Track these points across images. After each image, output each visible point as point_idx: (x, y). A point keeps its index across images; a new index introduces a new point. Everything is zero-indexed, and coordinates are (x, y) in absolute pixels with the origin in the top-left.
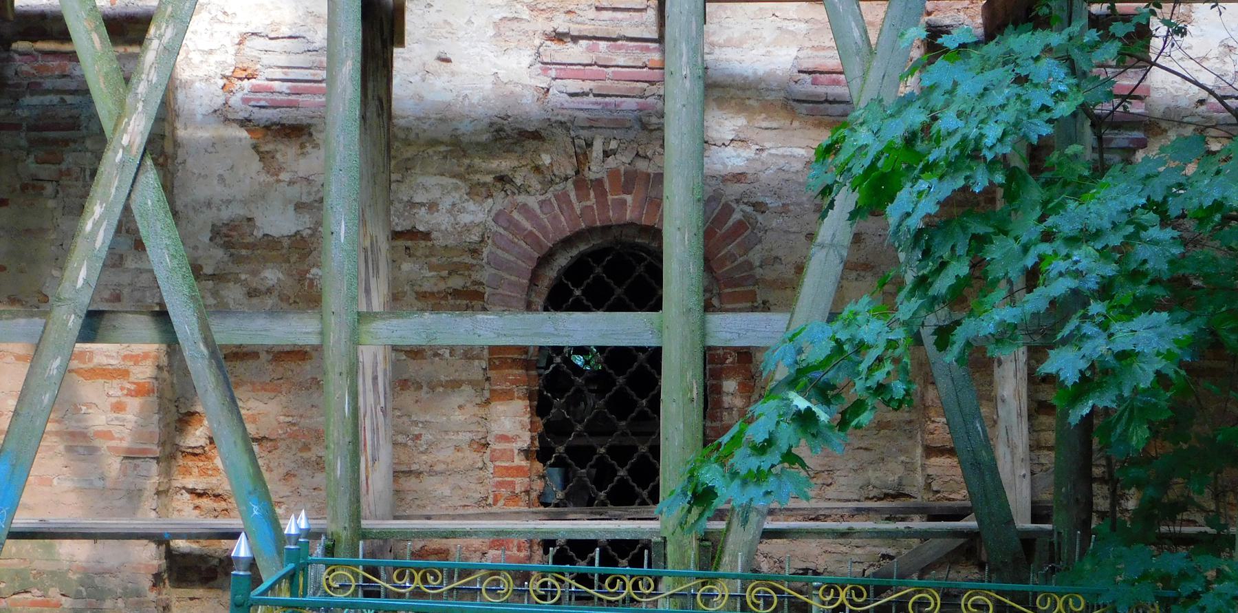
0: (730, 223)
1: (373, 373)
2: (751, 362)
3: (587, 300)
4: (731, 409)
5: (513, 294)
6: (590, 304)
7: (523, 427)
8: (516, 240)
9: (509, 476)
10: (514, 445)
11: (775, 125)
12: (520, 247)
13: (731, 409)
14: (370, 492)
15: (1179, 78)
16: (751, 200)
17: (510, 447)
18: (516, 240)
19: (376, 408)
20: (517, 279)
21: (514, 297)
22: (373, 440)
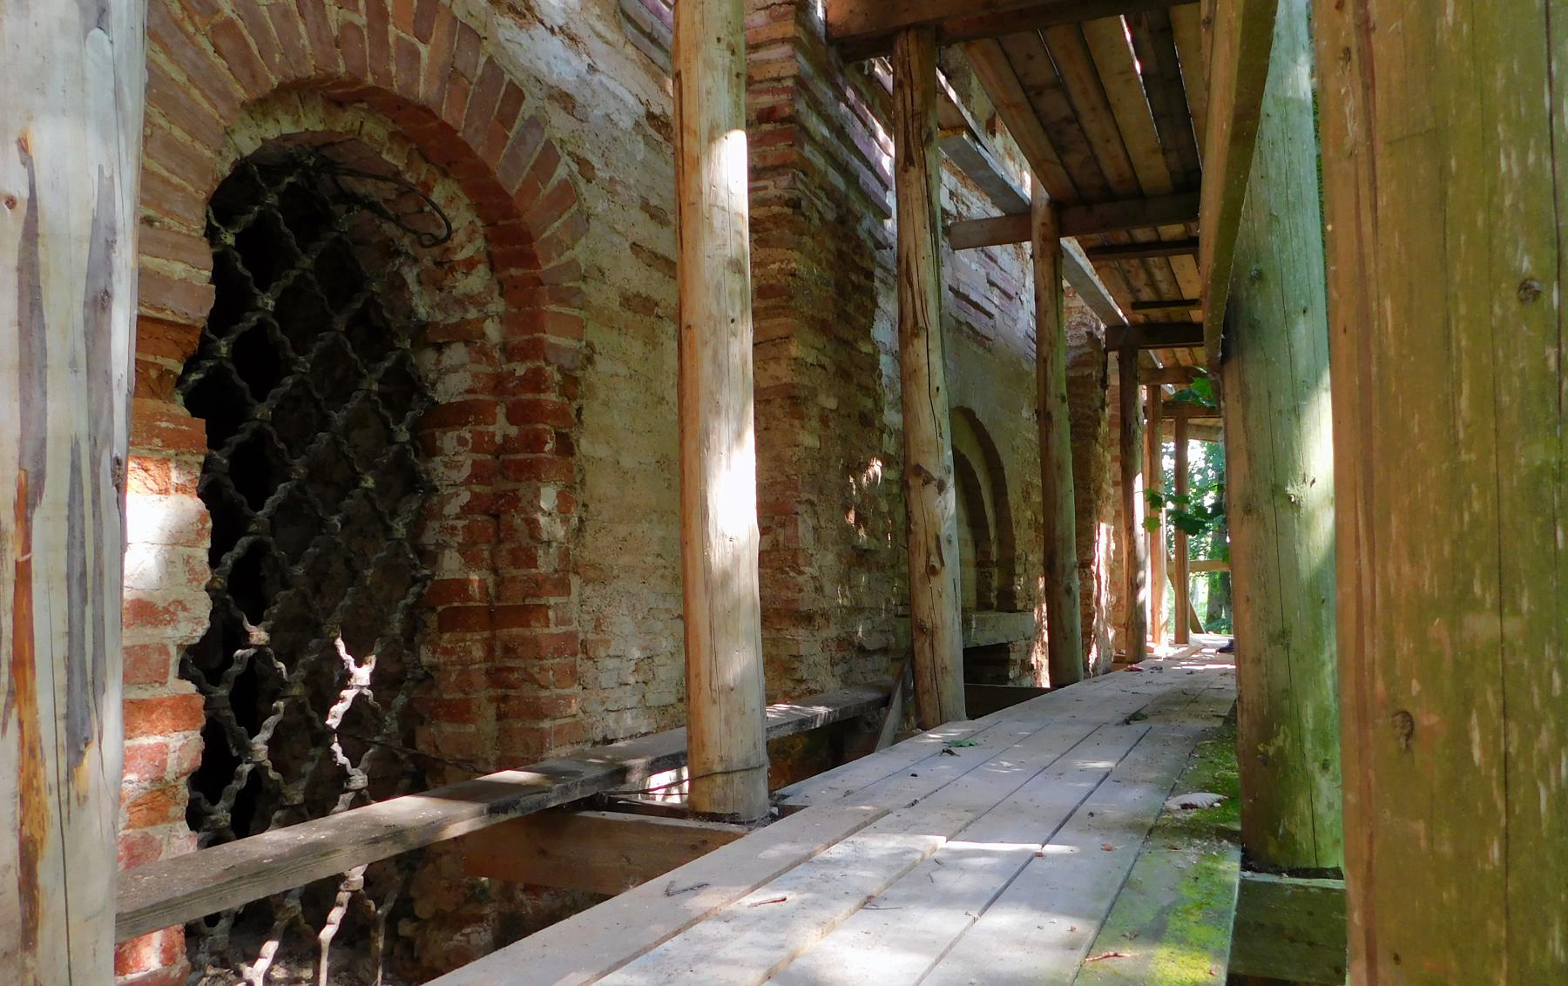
0: (554, 181)
1: (91, 276)
2: (572, 454)
3: (244, 264)
4: (549, 543)
5: (175, 180)
6: (248, 274)
7: (193, 576)
8: (191, 29)
9: (1483, 738)
10: (169, 631)
11: (609, 36)
12: (201, 52)
13: (549, 543)
14: (45, 934)
15: (1064, 172)
16: (578, 152)
17: (157, 640)
18: (191, 29)
19: (95, 463)
20: (188, 139)
21: (178, 188)
22: (73, 635)
